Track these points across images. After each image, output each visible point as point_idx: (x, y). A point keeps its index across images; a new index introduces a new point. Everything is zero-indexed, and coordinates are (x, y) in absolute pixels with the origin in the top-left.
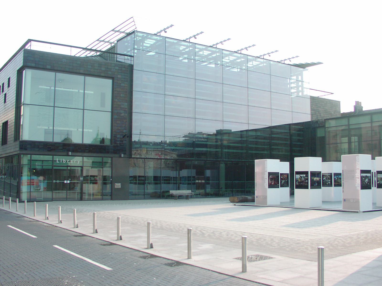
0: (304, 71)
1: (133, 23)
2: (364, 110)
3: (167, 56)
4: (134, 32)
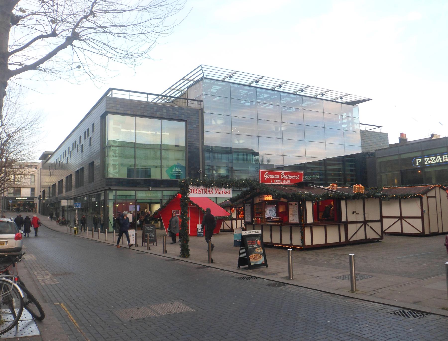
0: (354, 107)
1: (201, 72)
2: (408, 141)
3: (232, 100)
4: (202, 79)
